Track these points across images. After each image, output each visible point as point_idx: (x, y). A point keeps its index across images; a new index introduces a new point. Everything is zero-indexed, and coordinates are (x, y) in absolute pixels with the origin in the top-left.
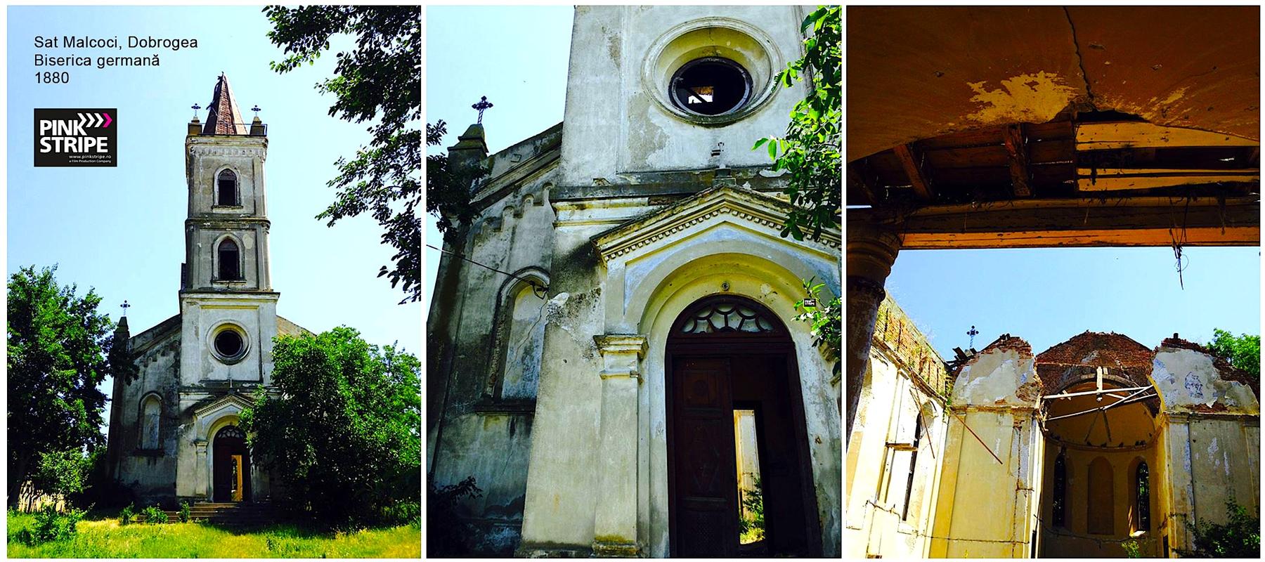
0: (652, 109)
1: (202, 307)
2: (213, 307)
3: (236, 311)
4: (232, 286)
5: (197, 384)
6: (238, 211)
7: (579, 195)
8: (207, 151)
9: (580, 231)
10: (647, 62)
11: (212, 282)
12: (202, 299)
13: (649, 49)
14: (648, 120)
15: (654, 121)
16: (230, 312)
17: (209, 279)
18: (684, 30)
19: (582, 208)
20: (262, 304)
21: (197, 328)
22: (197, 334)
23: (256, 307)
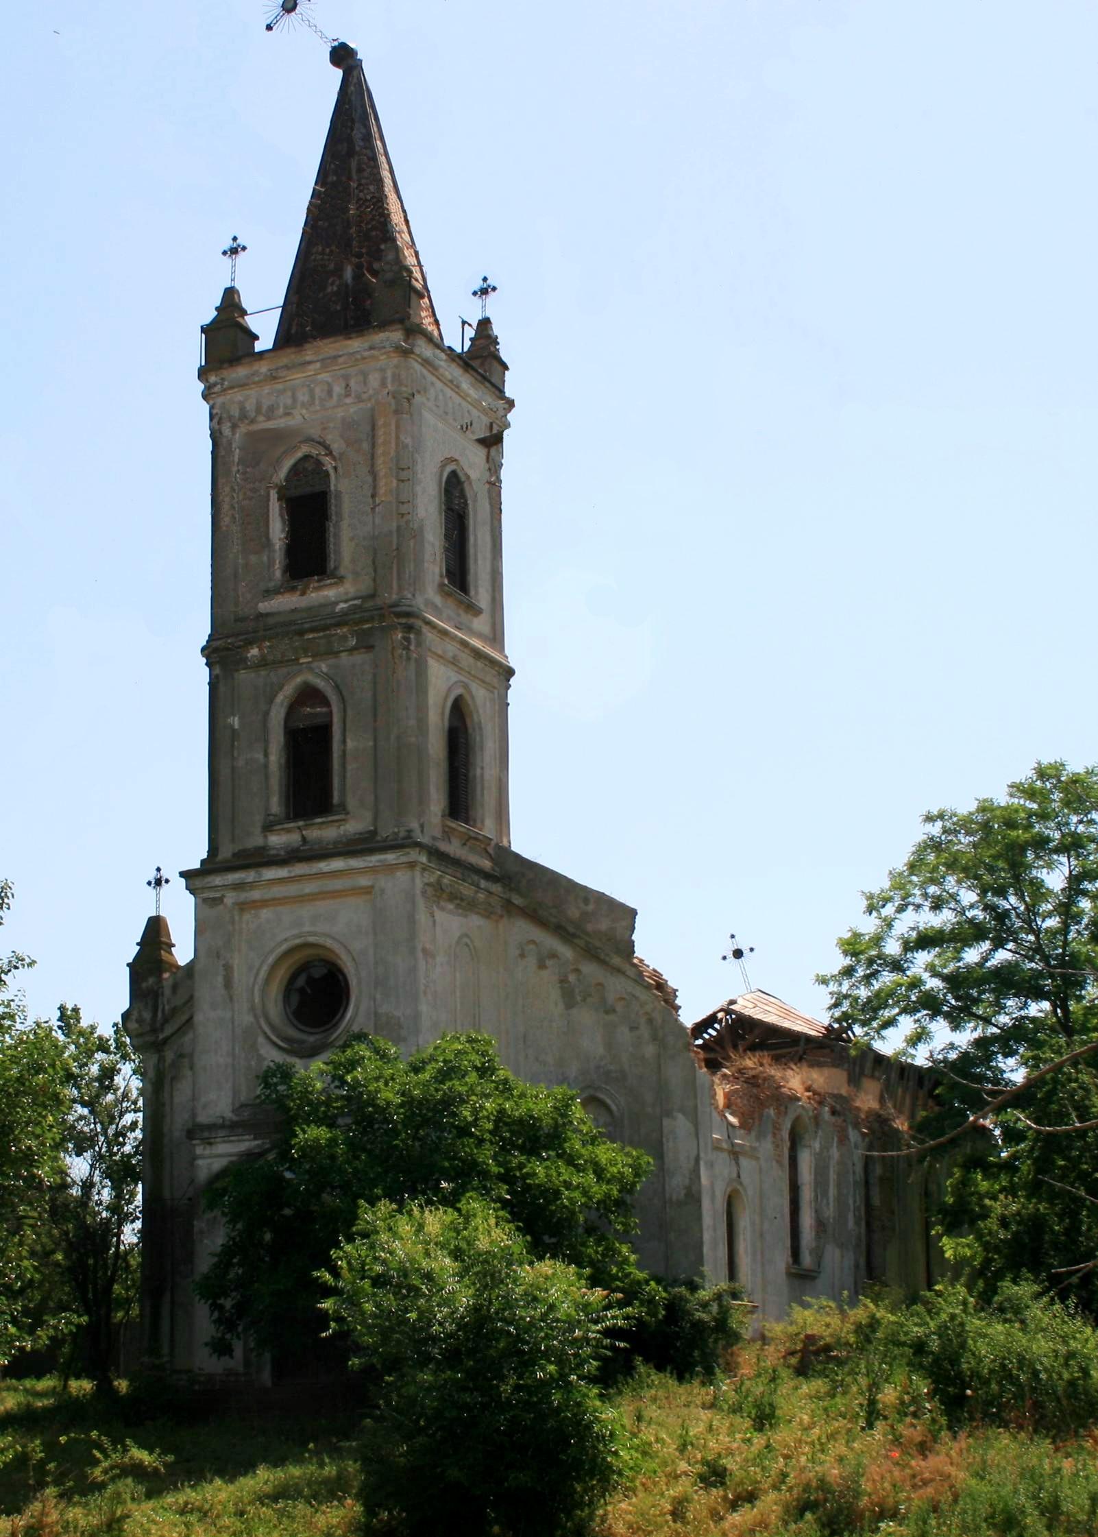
0: (261, 1040)
1: (243, 907)
2: (264, 903)
3: (322, 906)
4: (313, 834)
5: (229, 1114)
6: (330, 593)
7: (206, 1134)
8: (250, 406)
9: (210, 1164)
10: (257, 988)
11: (268, 828)
12: (239, 886)
13: (259, 970)
14: (257, 1050)
15: (262, 1052)
16: (306, 911)
17: (258, 819)
18: (284, 947)
19: (210, 1144)
20: (383, 882)
21: (228, 968)
22: (228, 984)
23: (368, 890)
